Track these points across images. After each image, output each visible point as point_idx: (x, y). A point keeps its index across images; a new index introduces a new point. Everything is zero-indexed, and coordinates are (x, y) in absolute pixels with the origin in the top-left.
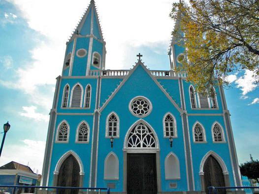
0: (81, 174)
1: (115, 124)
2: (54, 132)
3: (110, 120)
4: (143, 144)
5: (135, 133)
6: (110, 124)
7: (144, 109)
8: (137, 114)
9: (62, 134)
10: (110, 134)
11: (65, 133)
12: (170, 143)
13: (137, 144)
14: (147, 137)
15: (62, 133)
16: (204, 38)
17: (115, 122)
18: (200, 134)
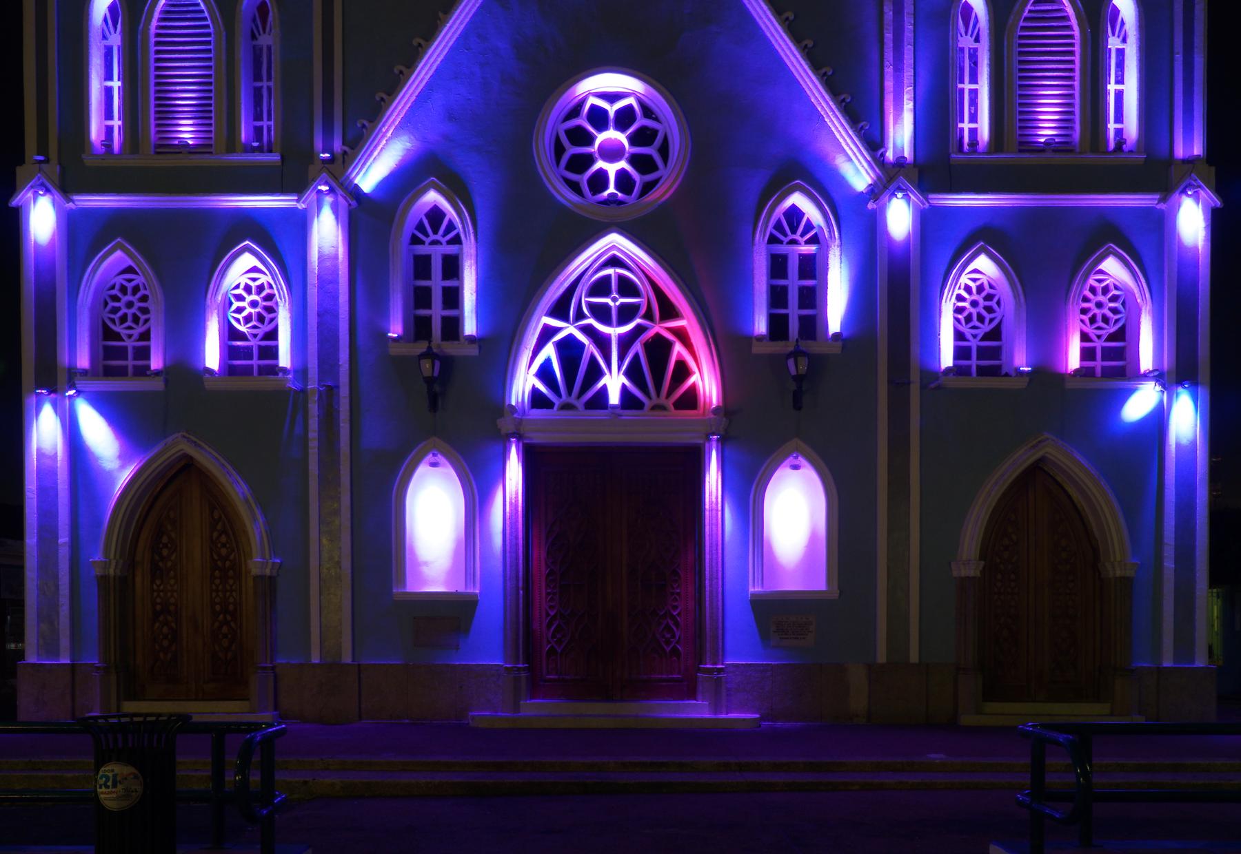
0: (255, 571)
7: (134, 315)
8: (662, 171)
9: (117, 337)
11: (139, 330)
12: (793, 386)
14: (647, 346)
15: (117, 328)
16: (265, 812)
17: (976, 45)
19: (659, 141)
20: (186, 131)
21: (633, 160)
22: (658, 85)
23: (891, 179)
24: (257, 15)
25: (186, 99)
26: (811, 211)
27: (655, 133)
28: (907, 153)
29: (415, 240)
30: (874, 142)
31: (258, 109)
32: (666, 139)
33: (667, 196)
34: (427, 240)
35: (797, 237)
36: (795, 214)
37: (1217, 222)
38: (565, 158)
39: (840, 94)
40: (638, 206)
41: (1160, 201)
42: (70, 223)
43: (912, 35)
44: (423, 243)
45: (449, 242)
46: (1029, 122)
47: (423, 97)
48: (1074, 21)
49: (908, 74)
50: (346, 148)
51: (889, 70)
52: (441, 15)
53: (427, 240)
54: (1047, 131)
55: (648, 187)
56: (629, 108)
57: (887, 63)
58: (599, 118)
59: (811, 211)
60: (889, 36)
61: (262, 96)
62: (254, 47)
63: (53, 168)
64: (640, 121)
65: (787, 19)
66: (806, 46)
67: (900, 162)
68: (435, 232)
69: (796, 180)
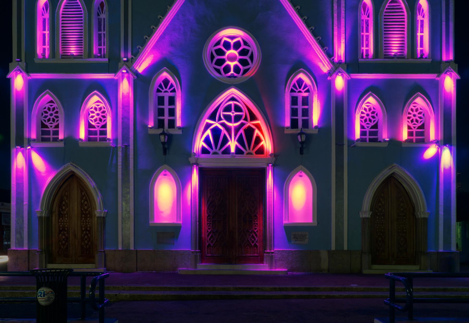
1: (172, 101)
2: (414, 191)
3: (158, 91)
4: (236, 146)
5: (216, 124)
6: (161, 100)
8: (251, 65)
9: (47, 127)
10: (160, 124)
13: (253, 149)
15: (47, 123)
17: (368, 18)
18: (372, 124)
19: (249, 54)
20: (73, 50)
23: (336, 68)
25: (73, 38)
28: (343, 58)
29: (158, 91)
30: (330, 54)
34: (163, 91)
35: (301, 90)
37: (459, 85)
42: (29, 84)
44: (161, 92)
46: (388, 47)
47: (162, 37)
48: (405, 10)
49: (343, 29)
51: (336, 28)
52: (168, 7)
53: (163, 91)
54: (395, 51)
63: (23, 64)
64: (243, 47)
65: (305, 19)
66: (298, 8)
67: (340, 63)
68: (166, 88)
69: (301, 68)
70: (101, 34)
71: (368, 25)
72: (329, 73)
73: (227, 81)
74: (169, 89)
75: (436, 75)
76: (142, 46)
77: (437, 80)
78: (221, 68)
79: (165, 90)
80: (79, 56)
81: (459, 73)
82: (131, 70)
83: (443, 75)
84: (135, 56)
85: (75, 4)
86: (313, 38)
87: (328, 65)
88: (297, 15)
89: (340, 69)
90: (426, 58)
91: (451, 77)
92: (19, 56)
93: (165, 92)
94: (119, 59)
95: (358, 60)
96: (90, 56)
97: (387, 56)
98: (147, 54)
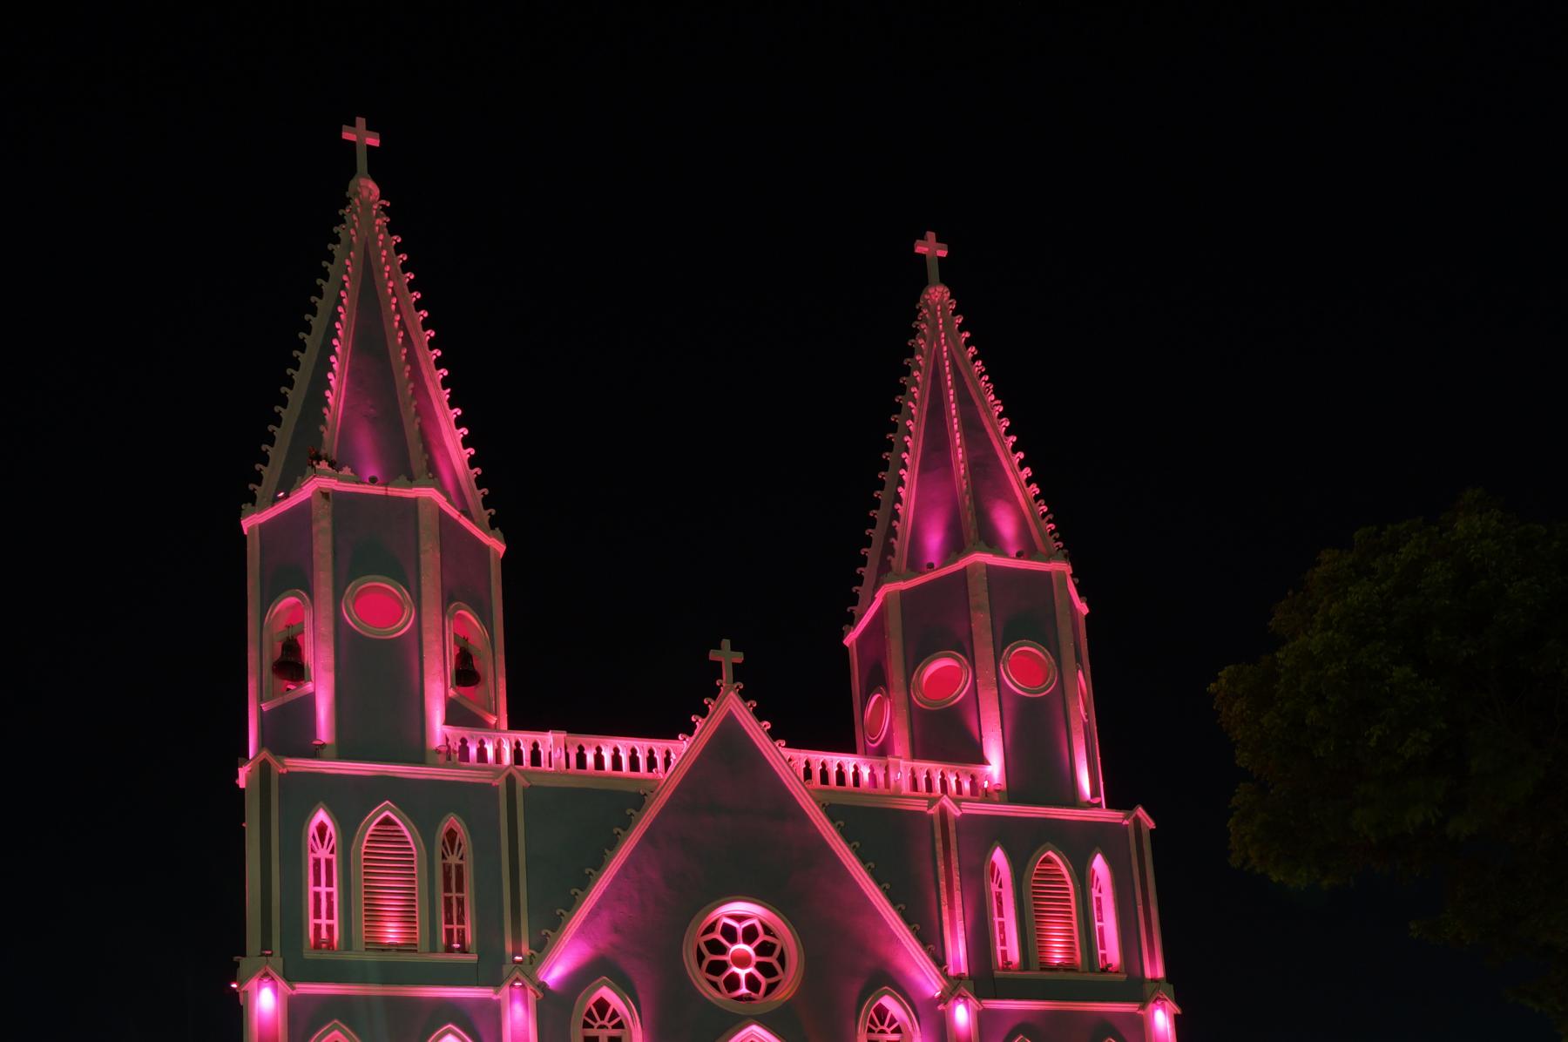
8: (781, 975)
17: (1000, 890)
19: (777, 953)
20: (392, 933)
21: (759, 966)
22: (770, 907)
23: (956, 987)
24: (446, 840)
25: (392, 904)
26: (615, 1001)
27: (774, 946)
28: (964, 969)
29: (586, 1025)
30: (939, 960)
31: (449, 915)
32: (782, 951)
33: (790, 996)
34: (596, 1025)
35: (885, 1028)
36: (602, 1006)
37: (1179, 1022)
38: (705, 964)
39: (883, 883)
40: (764, 1003)
41: (1140, 1008)
42: (294, 1009)
43: (959, 883)
44: (592, 1027)
45: (613, 1027)
46: (1043, 948)
47: (593, 914)
48: (1068, 878)
49: (959, 911)
50: (533, 952)
51: (945, 908)
52: (606, 851)
53: (596, 1025)
54: (1057, 957)
55: (771, 988)
56: (753, 927)
57: (943, 903)
58: (730, 933)
59: (615, 1001)
60: (943, 883)
61: (452, 905)
62: (444, 865)
63: (277, 961)
64: (762, 937)
65: (870, 867)
66: (885, 888)
67: (959, 977)
68: (602, 1018)
69: (884, 986)
70: (451, 897)
71: (1000, 902)
72: (943, 999)
73: (740, 1008)
74: (609, 1022)
75: (1138, 1005)
76: (553, 931)
77: (1140, 1014)
78: (720, 980)
79: (600, 1022)
80: (408, 947)
81: (1178, 1001)
82: (531, 980)
83: (1151, 1006)
84: (539, 952)
85: (391, 834)
86: (904, 927)
87: (938, 981)
88: (870, 881)
89: (963, 990)
90: (1117, 972)
91: (1164, 1011)
92: (266, 944)
93: (601, 1027)
94: (500, 959)
95: (992, 971)
96: (433, 950)
97: (1047, 967)
98: (563, 947)
